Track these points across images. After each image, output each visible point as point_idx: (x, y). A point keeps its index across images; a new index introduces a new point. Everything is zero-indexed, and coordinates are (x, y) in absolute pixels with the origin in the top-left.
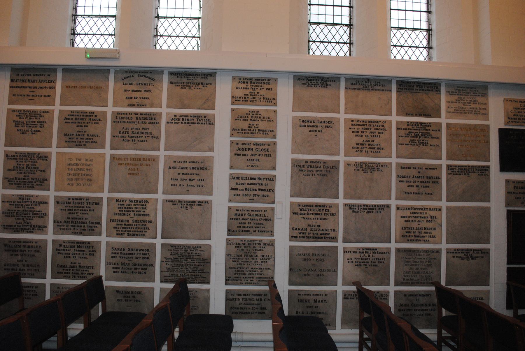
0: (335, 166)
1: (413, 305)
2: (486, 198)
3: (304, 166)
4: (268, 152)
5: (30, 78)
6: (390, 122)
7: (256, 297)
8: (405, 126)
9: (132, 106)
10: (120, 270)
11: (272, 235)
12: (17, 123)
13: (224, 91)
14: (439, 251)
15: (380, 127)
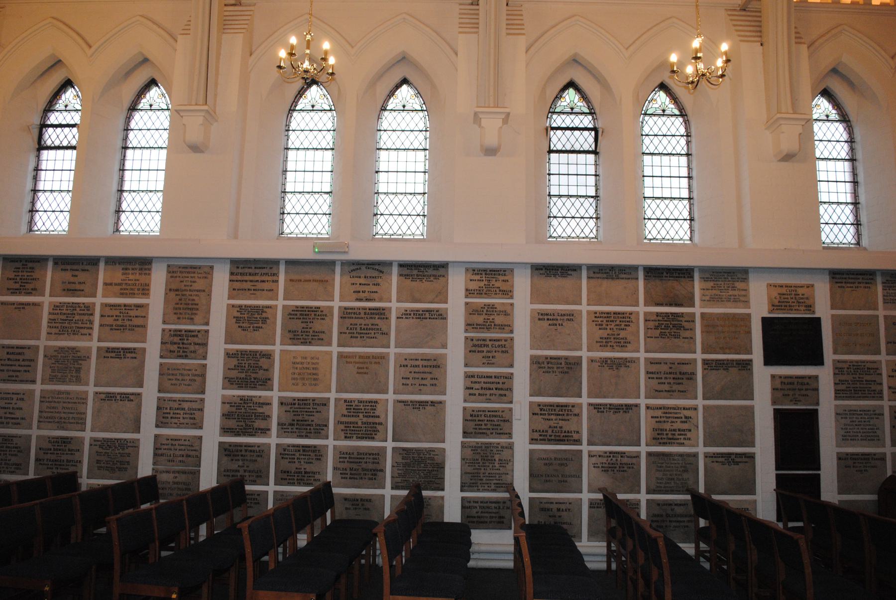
0: (578, 362)
1: (668, 515)
2: (749, 395)
3: (543, 363)
4: (505, 348)
5: (250, 271)
6: (638, 313)
7: (493, 505)
8: (655, 317)
9: (360, 300)
10: (348, 476)
11: (511, 437)
12: (238, 320)
13: (457, 283)
14: (695, 455)
15: (626, 319)
